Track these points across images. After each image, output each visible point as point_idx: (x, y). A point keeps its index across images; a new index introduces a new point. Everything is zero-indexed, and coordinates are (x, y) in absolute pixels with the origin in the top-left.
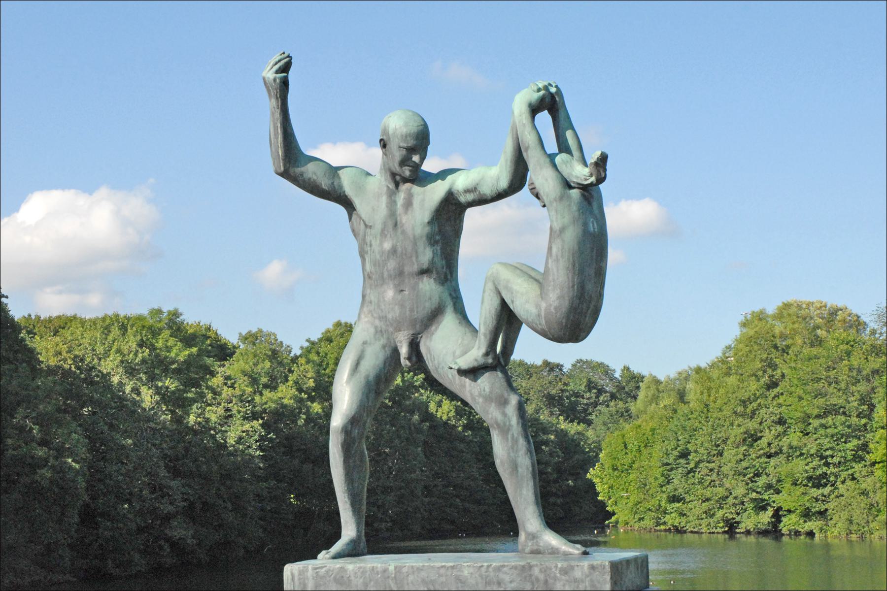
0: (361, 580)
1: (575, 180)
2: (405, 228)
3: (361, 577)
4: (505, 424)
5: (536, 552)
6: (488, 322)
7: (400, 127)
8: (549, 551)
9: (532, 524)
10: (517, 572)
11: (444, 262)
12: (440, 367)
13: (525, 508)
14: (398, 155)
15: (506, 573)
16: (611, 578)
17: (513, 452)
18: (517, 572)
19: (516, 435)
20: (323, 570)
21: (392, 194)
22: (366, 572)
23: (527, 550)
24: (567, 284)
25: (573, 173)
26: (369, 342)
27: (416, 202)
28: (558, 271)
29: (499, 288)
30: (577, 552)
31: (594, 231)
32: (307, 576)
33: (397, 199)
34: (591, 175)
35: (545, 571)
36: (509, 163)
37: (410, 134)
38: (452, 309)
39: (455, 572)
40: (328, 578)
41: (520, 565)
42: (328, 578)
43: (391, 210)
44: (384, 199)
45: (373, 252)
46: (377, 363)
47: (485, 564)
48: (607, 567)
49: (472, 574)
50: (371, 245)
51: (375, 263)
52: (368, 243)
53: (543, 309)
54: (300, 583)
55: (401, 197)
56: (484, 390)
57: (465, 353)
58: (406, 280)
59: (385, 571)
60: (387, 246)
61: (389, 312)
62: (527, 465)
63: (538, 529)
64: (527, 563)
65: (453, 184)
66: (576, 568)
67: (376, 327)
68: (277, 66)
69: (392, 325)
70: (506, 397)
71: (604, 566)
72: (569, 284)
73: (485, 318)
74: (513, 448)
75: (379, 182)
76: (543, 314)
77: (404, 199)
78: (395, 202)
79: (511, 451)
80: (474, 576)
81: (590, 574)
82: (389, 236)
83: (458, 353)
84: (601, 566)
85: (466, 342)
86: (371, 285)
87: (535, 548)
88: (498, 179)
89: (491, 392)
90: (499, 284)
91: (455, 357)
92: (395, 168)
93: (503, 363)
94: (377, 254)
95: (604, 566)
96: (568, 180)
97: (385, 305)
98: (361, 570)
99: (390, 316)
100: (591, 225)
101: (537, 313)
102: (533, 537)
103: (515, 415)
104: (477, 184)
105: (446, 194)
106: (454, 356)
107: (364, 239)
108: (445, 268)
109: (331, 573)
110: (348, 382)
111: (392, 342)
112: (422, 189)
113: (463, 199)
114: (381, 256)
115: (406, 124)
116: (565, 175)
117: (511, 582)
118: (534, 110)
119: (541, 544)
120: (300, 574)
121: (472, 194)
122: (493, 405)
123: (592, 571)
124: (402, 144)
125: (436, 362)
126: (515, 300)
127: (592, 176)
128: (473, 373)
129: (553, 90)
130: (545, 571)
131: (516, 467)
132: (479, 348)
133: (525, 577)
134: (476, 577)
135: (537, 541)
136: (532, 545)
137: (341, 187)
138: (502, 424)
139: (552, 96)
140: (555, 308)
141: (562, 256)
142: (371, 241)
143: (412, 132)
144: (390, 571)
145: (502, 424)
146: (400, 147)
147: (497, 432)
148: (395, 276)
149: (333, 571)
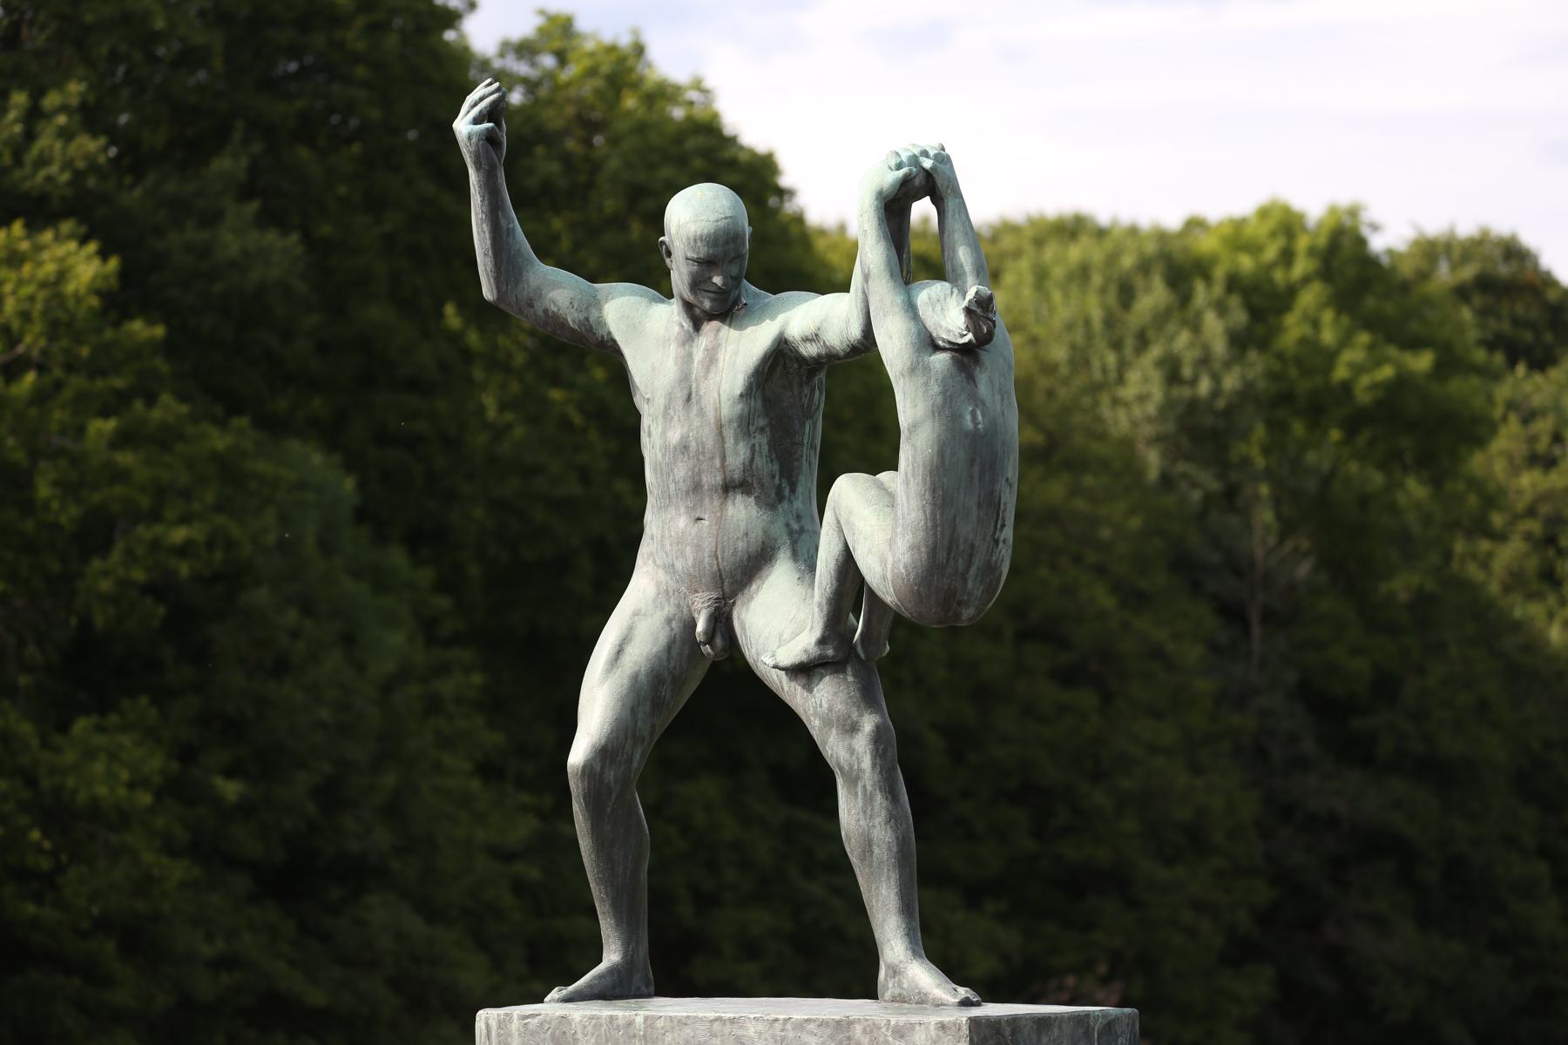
4: (851, 767)
10: (829, 1031)
11: (776, 467)
13: (884, 920)
19: (869, 788)
21: (688, 340)
22: (601, 1025)
24: (922, 523)
26: (643, 612)
27: (724, 357)
35: (871, 1032)
38: (788, 553)
40: (542, 1036)
45: (653, 447)
46: (655, 650)
55: (703, 341)
58: (707, 499)
60: (675, 436)
65: (786, 324)
66: (918, 1028)
72: (926, 524)
74: (865, 812)
80: (763, 1037)
82: (676, 418)
83: (786, 636)
84: (955, 1024)
87: (897, 991)
95: (959, 1024)
96: (934, 335)
99: (679, 565)
100: (968, 417)
103: (868, 752)
108: (777, 477)
114: (664, 456)
122: (834, 731)
124: (690, 255)
130: (871, 1032)
135: (900, 981)
137: (601, 323)
140: (906, 567)
146: (687, 259)
148: (687, 492)
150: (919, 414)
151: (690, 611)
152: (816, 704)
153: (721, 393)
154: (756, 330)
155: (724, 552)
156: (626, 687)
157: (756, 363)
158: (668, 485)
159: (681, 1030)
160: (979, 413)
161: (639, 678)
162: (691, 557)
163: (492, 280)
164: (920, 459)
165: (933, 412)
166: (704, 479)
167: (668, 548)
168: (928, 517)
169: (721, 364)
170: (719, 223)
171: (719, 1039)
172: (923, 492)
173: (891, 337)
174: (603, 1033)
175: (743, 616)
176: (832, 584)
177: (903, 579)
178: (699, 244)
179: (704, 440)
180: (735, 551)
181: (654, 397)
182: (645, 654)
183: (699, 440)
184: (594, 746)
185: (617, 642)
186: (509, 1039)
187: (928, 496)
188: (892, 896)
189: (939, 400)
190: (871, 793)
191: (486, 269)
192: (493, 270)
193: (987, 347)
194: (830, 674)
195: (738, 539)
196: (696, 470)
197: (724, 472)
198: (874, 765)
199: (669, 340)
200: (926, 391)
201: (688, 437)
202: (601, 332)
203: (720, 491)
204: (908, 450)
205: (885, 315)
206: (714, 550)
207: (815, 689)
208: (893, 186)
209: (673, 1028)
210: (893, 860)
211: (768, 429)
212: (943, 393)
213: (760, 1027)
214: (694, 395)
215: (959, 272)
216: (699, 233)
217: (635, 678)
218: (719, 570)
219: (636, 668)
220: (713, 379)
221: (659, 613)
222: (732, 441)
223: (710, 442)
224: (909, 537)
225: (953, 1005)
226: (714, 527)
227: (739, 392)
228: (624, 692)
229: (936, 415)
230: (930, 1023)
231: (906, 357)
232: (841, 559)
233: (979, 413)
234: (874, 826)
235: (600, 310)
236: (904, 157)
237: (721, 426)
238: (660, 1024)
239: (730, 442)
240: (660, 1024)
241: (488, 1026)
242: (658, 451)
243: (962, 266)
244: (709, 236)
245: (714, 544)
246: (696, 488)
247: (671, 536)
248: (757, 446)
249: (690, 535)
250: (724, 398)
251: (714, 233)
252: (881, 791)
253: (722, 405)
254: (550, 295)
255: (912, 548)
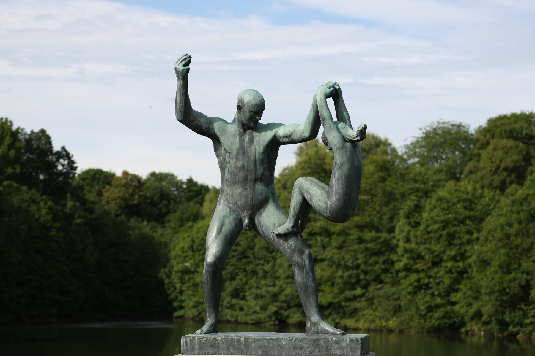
0: (225, 345)
1: (349, 138)
2: (249, 155)
3: (225, 344)
4: (302, 264)
5: (317, 333)
6: (295, 209)
7: (251, 100)
8: (324, 332)
9: (314, 318)
10: (311, 342)
11: (269, 174)
12: (266, 231)
13: (311, 309)
14: (248, 115)
15: (305, 343)
16: (361, 347)
17: (306, 279)
18: (311, 342)
19: (308, 270)
20: (204, 340)
21: (242, 135)
22: (228, 341)
23: (311, 331)
24: (342, 192)
25: (348, 134)
26: (226, 216)
27: (256, 140)
28: (338, 185)
29: (303, 191)
30: (339, 333)
31: (357, 165)
32: (195, 343)
33: (245, 138)
34: (357, 136)
35: (326, 342)
36: (310, 124)
37: (256, 105)
38: (272, 200)
39: (278, 342)
40: (206, 344)
41: (313, 339)
42: (206, 344)
43: (242, 144)
44: (238, 138)
45: (231, 167)
46: (231, 228)
47: (294, 338)
48: (359, 341)
49: (287, 343)
50: (229, 163)
51: (231, 173)
52: (228, 162)
53: (329, 205)
54: (191, 346)
55: (247, 137)
56: (291, 246)
57: (280, 225)
58: (249, 183)
59: (239, 340)
60: (239, 164)
61: (238, 201)
62: (313, 287)
63: (318, 320)
64: (317, 338)
65: (277, 132)
66: (343, 341)
67: (230, 208)
68: (184, 62)
69: (239, 207)
70: (303, 250)
71: (358, 340)
72: (343, 193)
73: (294, 207)
74: (306, 278)
75: (234, 129)
76: (329, 207)
77: (249, 138)
78: (244, 140)
79: (305, 279)
80: (288, 344)
81: (350, 344)
82: (240, 159)
83: (276, 225)
84: (356, 340)
85: (280, 219)
86: (228, 185)
87: (316, 330)
88: (303, 132)
89: (295, 247)
90: (303, 189)
91: (275, 227)
92: (245, 122)
93: (301, 231)
94: (233, 168)
95: (358, 340)
96: (345, 137)
97: (236, 196)
98: (225, 340)
99: (239, 203)
100: (356, 162)
101: (325, 207)
102: (315, 324)
103: (308, 260)
104: (291, 134)
105: (272, 137)
106: (274, 226)
107: (225, 159)
108: (269, 178)
109: (208, 341)
110: (216, 238)
111: (239, 217)
112: (259, 134)
113: (281, 140)
114: (235, 170)
115: (254, 99)
116: (343, 133)
117: (308, 348)
118: (327, 97)
119: (320, 328)
120: (190, 342)
121: (287, 138)
122: (296, 253)
123: (351, 343)
124: (251, 110)
125: (264, 229)
126: (312, 199)
127: (358, 137)
128: (285, 236)
129: (337, 87)
130: (326, 342)
131: (307, 287)
132: (290, 223)
133: (316, 345)
134: (289, 345)
135: (317, 327)
136: (314, 328)
137: (213, 129)
138: (301, 264)
139: (336, 89)
140: (336, 205)
141: (341, 178)
142: (229, 161)
143: (257, 103)
144: (242, 341)
145: (301, 264)
146: (250, 111)
147: (297, 268)
148: (243, 181)
149: (209, 340)
150: (344, 161)
151: (240, 216)
152: (289, 245)
153: (256, 151)
154: (265, 133)
155: (255, 199)
156: (224, 239)
157: (267, 143)
158: (236, 178)
159: (258, 342)
160: (358, 161)
161: (227, 236)
162: (244, 200)
163: (182, 114)
164: (344, 174)
165: (348, 160)
166: (249, 177)
167: (235, 197)
168: (344, 191)
169: (255, 143)
170: (261, 101)
171: (272, 345)
172: (343, 183)
173: (335, 137)
174: (229, 343)
175: (259, 218)
176: (298, 210)
177: (334, 209)
178: (255, 107)
179: (250, 165)
180: (258, 199)
181: (232, 152)
182: (228, 229)
183: (248, 165)
184: (216, 256)
185: (220, 225)
186: (194, 345)
187: (345, 185)
188: (314, 302)
189: (350, 156)
190: (308, 272)
191: (181, 111)
192: (184, 111)
193: (70, 155)
194: (294, 236)
195: (259, 195)
196: (246, 174)
197: (256, 175)
198: (309, 264)
199: (236, 135)
200: (346, 154)
201: (245, 164)
202: (213, 132)
203: (253, 181)
204: (339, 171)
205: (331, 131)
206: (252, 198)
207: (289, 241)
208: (329, 93)
209: (255, 342)
210: (314, 292)
211: (268, 163)
212: (350, 154)
213: (287, 341)
214: (246, 152)
215: (344, 119)
216: (255, 103)
217: (226, 236)
218: (253, 205)
219: (226, 233)
220: (253, 148)
221: (231, 217)
222: (259, 166)
223: (252, 166)
224: (338, 196)
225: (340, 334)
226: (252, 191)
227: (262, 152)
228: (224, 240)
229: (349, 161)
230: (347, 340)
231: (340, 143)
232: (302, 202)
233: (358, 161)
234: (309, 282)
235: (213, 125)
236: (331, 85)
237: (256, 161)
238: (250, 340)
239: (258, 167)
240: (250, 340)
241: (186, 342)
242: (233, 168)
243: (345, 117)
244: (258, 104)
245: (252, 197)
246: (246, 180)
247: (236, 194)
248: (265, 168)
249: (243, 194)
250: (257, 154)
251: (260, 103)
252: (311, 271)
253: (256, 155)
254: (199, 120)
255: (338, 200)
